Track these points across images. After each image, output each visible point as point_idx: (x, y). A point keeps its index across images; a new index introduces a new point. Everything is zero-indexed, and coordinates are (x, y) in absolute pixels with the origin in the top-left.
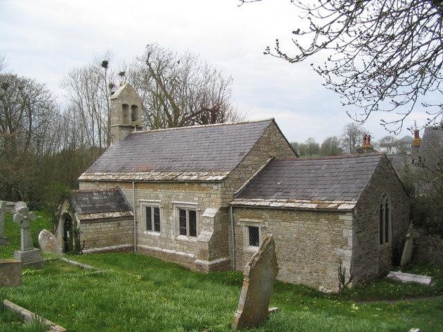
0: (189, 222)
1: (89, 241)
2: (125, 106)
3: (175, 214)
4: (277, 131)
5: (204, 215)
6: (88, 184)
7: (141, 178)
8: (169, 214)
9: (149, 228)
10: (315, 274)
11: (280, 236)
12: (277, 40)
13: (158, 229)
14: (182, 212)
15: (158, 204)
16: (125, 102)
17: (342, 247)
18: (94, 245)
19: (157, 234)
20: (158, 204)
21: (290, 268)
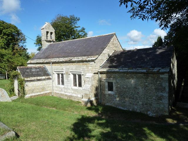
0: (78, 80)
1: (29, 90)
2: (47, 32)
3: (72, 76)
4: (116, 39)
5: (86, 77)
6: (31, 65)
7: (55, 61)
8: (68, 78)
9: (59, 83)
10: (145, 106)
11: (125, 86)
12: (120, 6)
13: (63, 84)
14: (75, 75)
15: (80, 73)
16: (47, 30)
17: (162, 92)
18: (33, 92)
19: (63, 86)
20: (80, 73)
21: (131, 102)
